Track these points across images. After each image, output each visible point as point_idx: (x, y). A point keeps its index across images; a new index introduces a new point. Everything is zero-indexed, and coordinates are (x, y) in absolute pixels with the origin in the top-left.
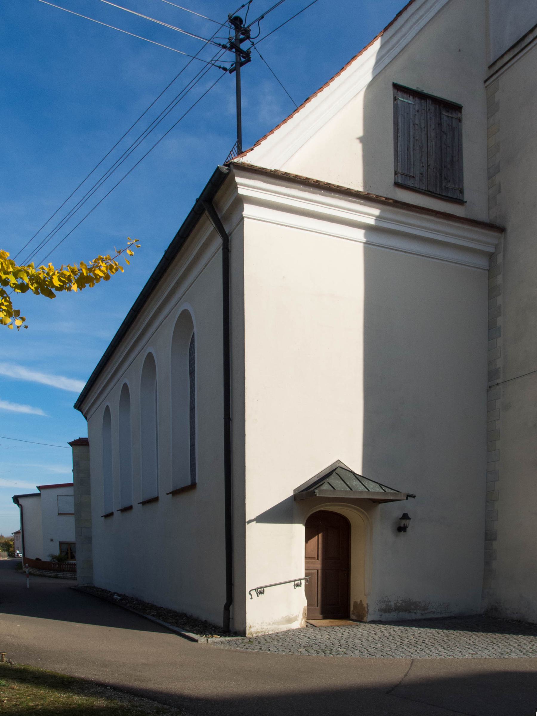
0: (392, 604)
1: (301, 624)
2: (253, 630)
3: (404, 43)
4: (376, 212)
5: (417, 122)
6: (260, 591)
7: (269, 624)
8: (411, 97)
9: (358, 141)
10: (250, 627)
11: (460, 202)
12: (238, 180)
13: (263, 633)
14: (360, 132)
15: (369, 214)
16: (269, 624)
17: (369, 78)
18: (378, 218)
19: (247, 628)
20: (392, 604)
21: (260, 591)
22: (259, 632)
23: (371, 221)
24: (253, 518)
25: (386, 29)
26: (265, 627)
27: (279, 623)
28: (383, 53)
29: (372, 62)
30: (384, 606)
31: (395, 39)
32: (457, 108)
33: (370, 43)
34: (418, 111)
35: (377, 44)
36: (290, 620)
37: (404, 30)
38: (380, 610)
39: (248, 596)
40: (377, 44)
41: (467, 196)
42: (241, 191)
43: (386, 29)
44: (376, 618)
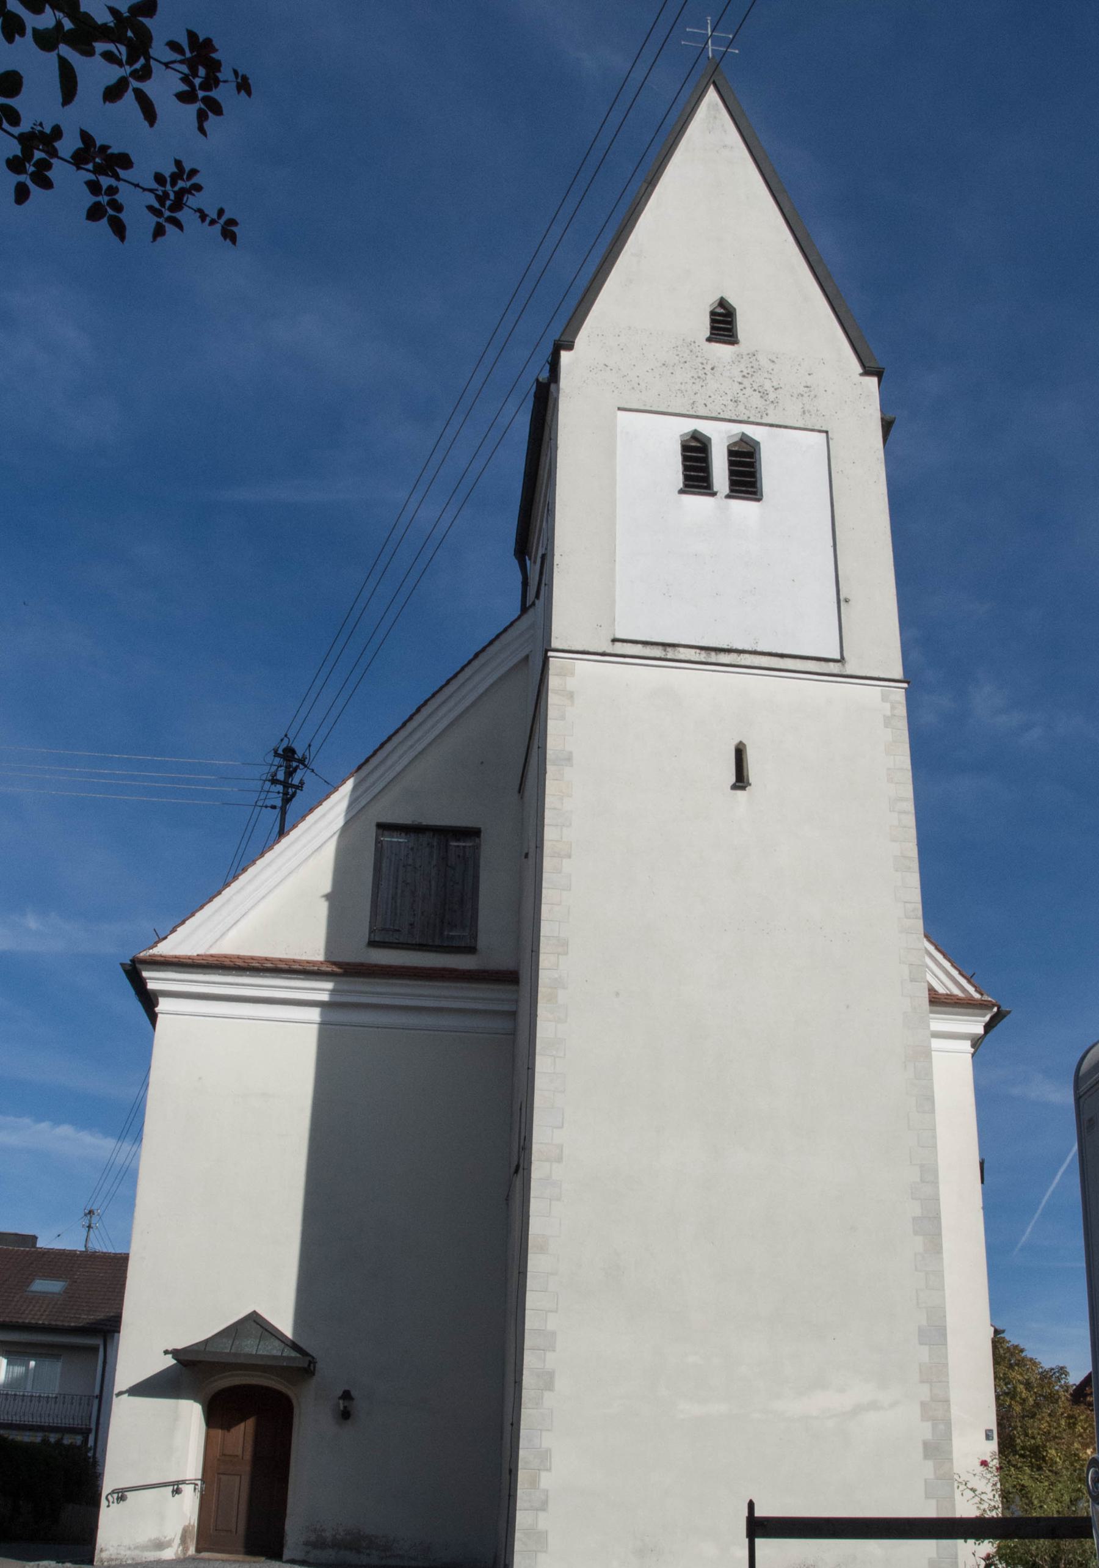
0: (328, 1535)
1: (176, 1553)
2: (104, 1555)
3: (420, 748)
4: (329, 985)
5: (410, 862)
6: (121, 1495)
7: (129, 1549)
8: (403, 834)
9: (323, 899)
10: (101, 1550)
11: (471, 950)
12: (145, 974)
13: (118, 1562)
14: (327, 887)
15: (322, 990)
16: (129, 1549)
17: (340, 822)
18: (333, 992)
19: (97, 1552)
20: (328, 1535)
21: (121, 1495)
22: (112, 1560)
23: (325, 997)
24: (124, 1389)
25: (359, 768)
26: (123, 1553)
27: (145, 1548)
28: (358, 793)
29: (344, 804)
30: (313, 1538)
31: (371, 780)
32: (473, 833)
33: (344, 782)
34: (412, 849)
35: (349, 784)
36: (160, 1545)
37: (389, 763)
38: (307, 1543)
39: (104, 1503)
40: (349, 784)
41: (482, 942)
42: (151, 986)
43: (359, 768)
44: (298, 1556)
